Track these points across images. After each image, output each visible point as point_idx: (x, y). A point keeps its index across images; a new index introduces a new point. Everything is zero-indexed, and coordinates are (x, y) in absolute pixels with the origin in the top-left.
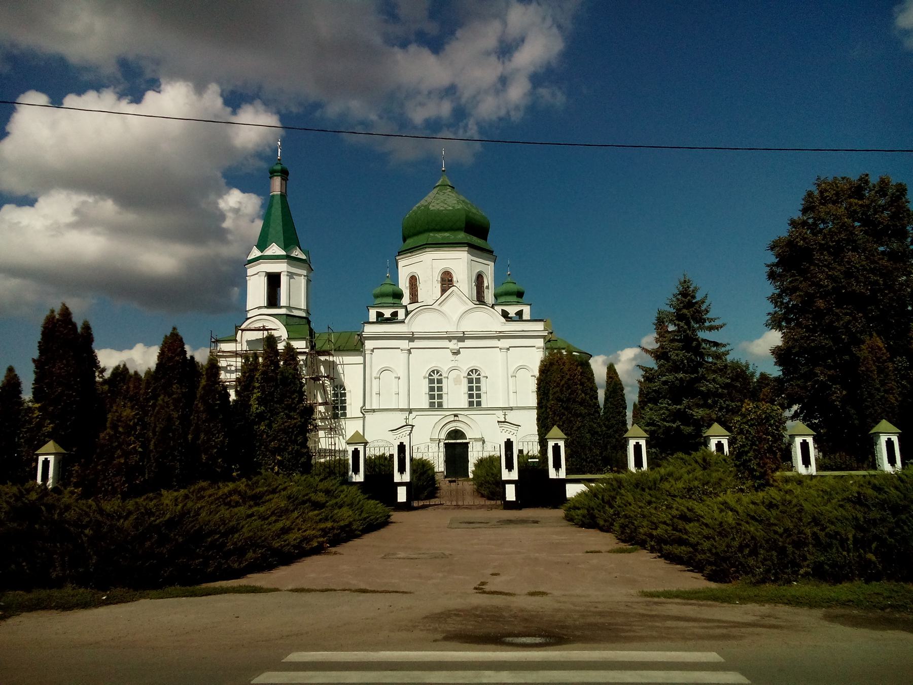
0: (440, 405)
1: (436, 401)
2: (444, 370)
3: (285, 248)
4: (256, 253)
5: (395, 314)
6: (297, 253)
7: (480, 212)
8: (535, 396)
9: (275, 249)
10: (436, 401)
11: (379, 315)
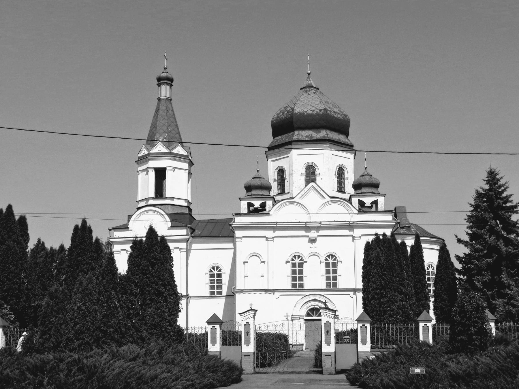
0: (301, 285)
1: (297, 285)
4: (145, 152)
5: (263, 205)
6: (179, 150)
7: (335, 111)
9: (160, 148)
10: (297, 282)
11: (250, 205)
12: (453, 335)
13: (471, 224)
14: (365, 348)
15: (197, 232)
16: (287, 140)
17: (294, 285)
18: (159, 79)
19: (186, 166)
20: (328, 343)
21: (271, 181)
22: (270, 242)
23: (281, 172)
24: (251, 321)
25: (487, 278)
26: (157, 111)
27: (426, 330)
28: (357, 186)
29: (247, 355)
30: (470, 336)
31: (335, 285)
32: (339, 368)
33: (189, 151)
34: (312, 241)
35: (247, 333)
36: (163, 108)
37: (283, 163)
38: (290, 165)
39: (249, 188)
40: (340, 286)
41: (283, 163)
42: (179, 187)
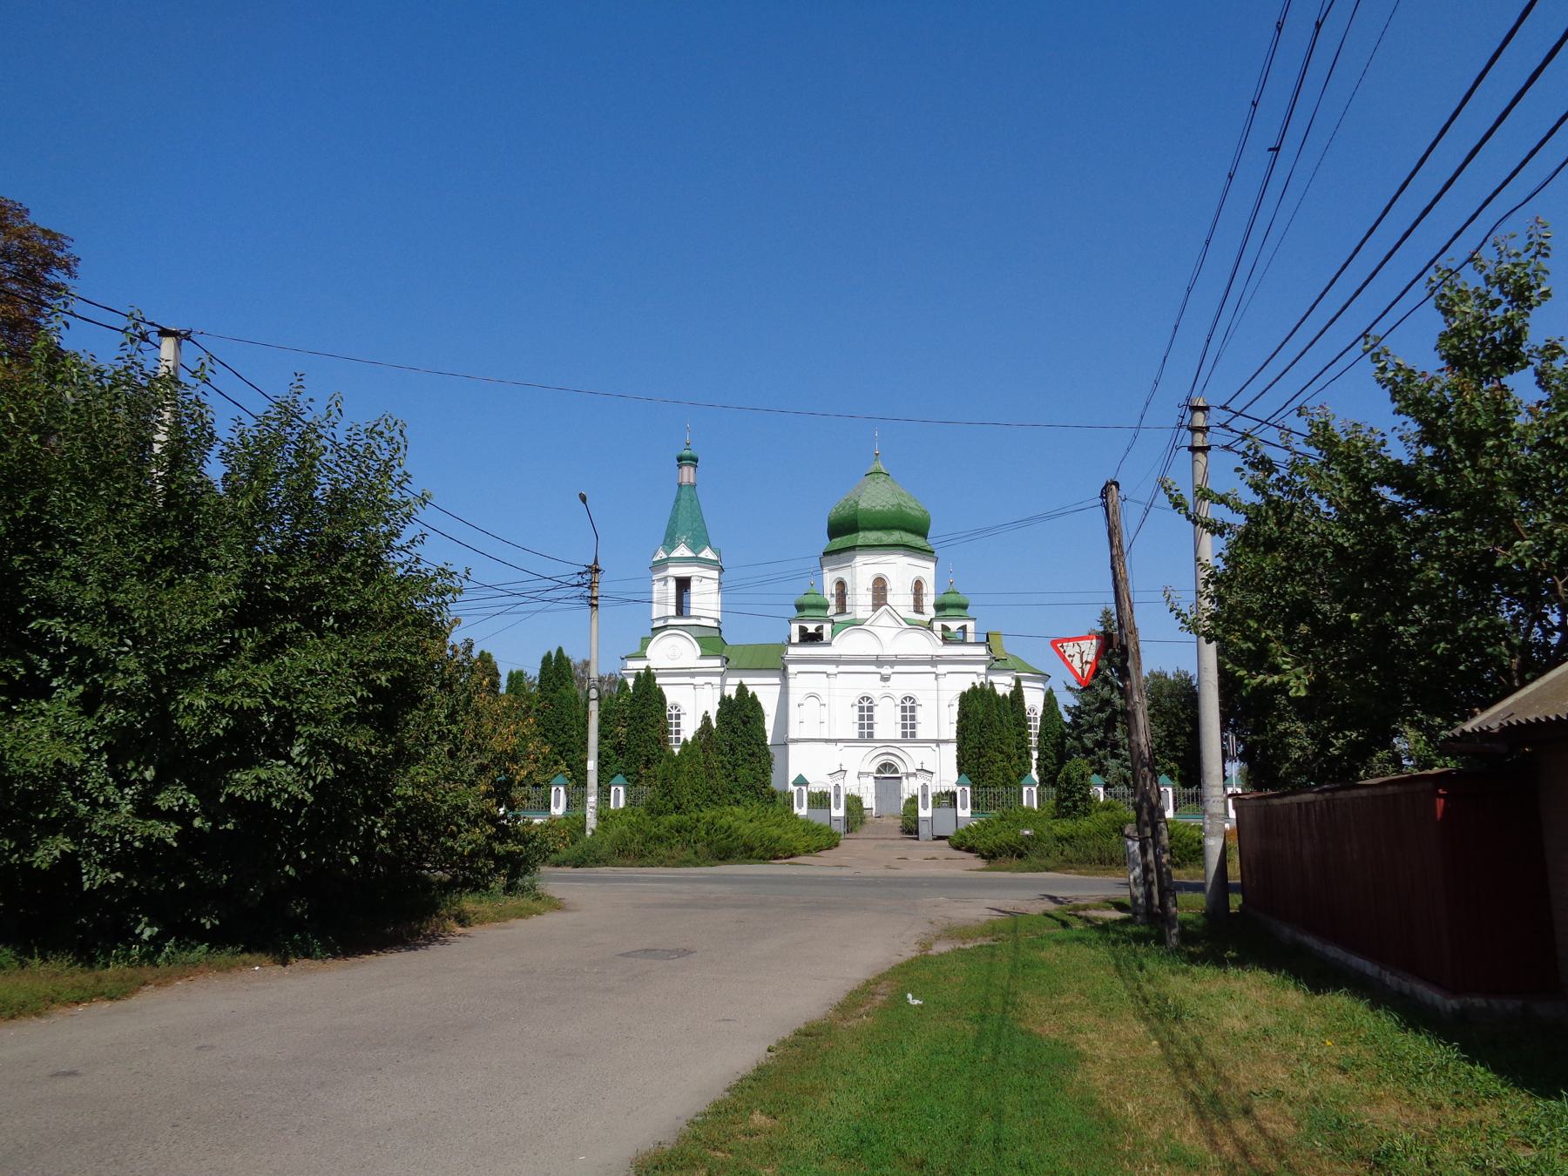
0: (871, 735)
1: (867, 734)
2: (876, 695)
3: (692, 548)
4: (662, 555)
6: (707, 554)
7: (913, 506)
8: (954, 727)
9: (682, 551)
11: (803, 630)
12: (1060, 801)
13: (1067, 719)
14: (965, 813)
15: (732, 663)
16: (849, 544)
17: (861, 735)
18: (680, 459)
19: (715, 574)
20: (925, 808)
21: (828, 597)
22: (832, 679)
23: (841, 584)
24: (840, 783)
25: (1100, 735)
26: (677, 500)
27: (1030, 795)
28: (939, 607)
29: (837, 819)
30: (1075, 802)
31: (913, 734)
32: (937, 833)
33: (719, 556)
34: (885, 679)
35: (837, 796)
36: (685, 496)
37: (843, 574)
38: (853, 576)
39: (800, 607)
40: (919, 736)
41: (843, 574)
42: (706, 601)
